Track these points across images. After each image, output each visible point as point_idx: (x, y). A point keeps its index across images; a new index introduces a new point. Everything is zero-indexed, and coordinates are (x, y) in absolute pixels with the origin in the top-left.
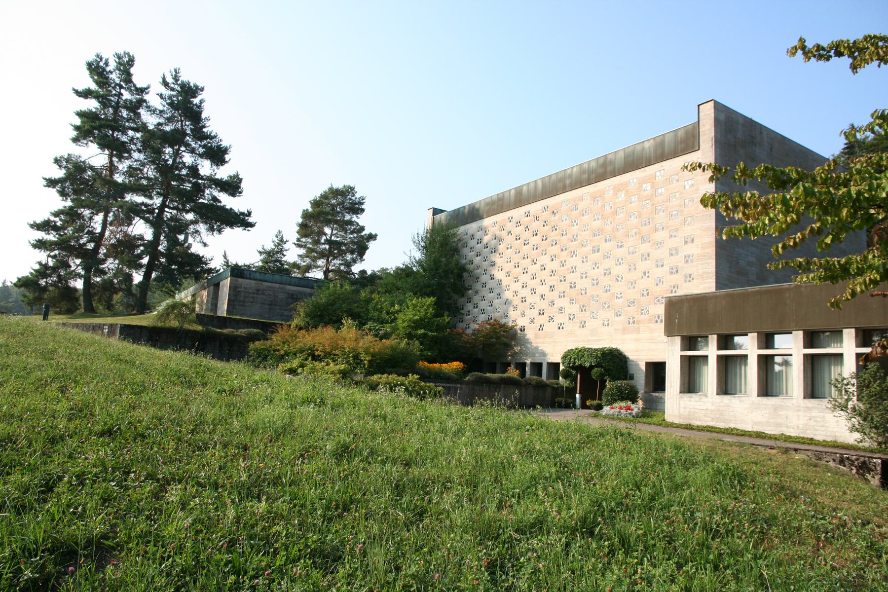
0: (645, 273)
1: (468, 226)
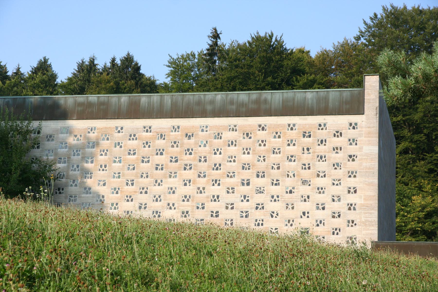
0: (245, 197)
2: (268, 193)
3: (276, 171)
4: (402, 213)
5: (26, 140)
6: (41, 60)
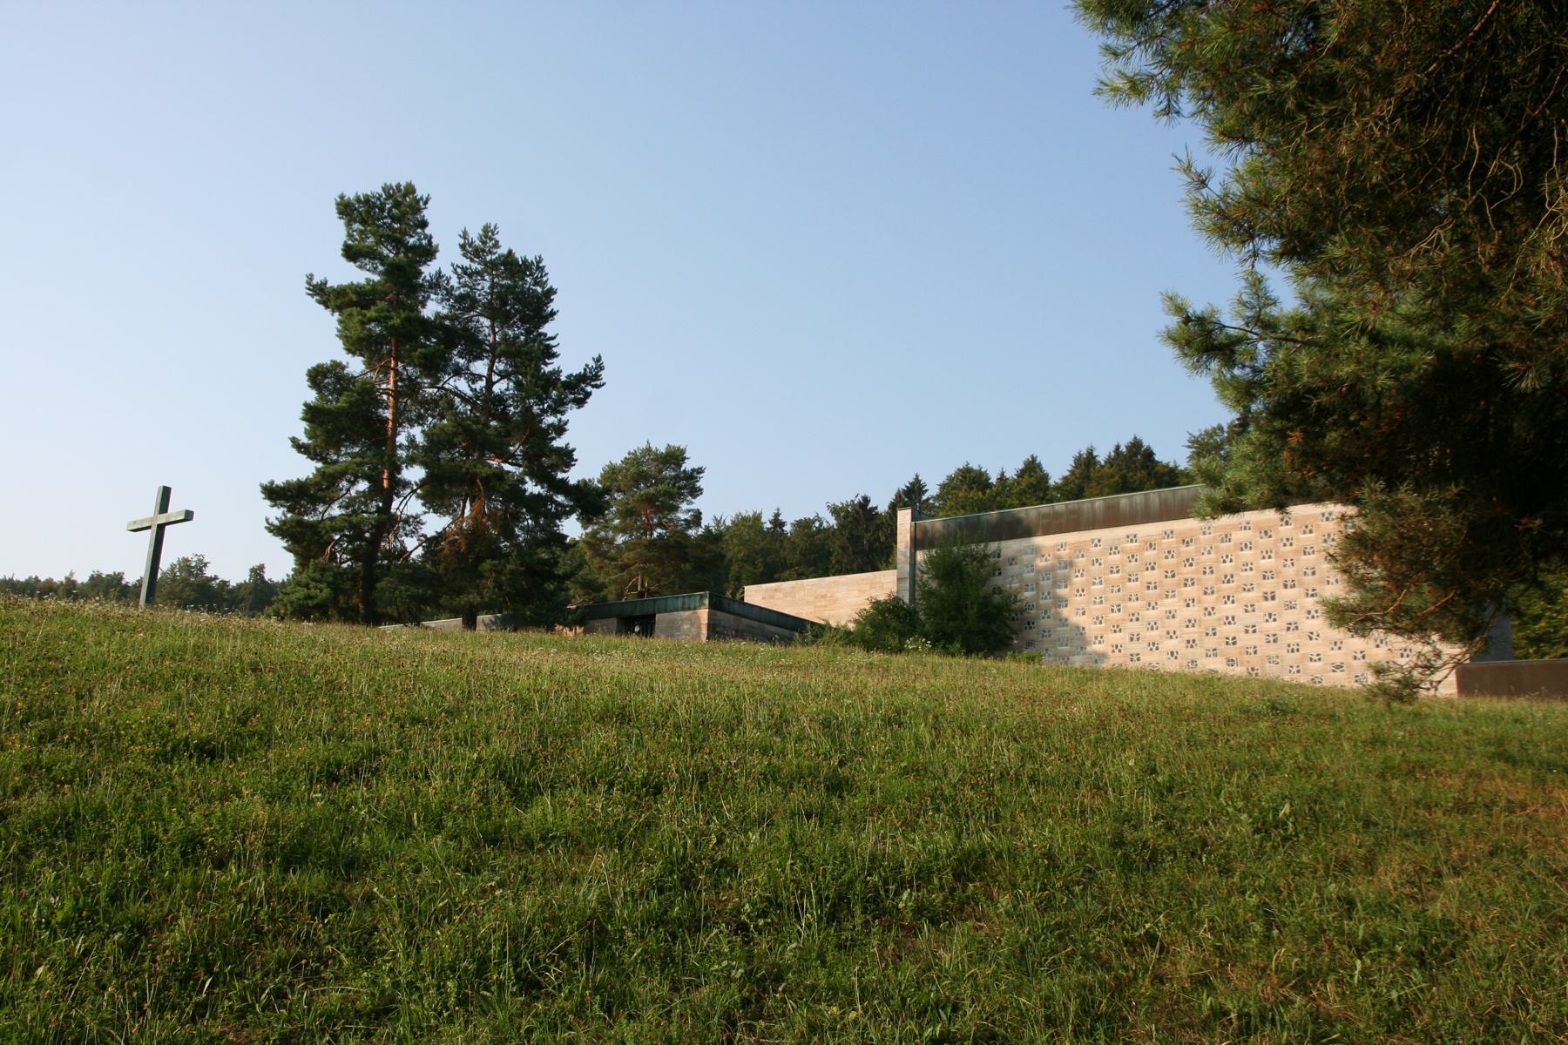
0: (1270, 615)
1: (1004, 544)
2: (1302, 608)
3: (1311, 578)
4: (1548, 614)
5: (982, 566)
6: (757, 518)
